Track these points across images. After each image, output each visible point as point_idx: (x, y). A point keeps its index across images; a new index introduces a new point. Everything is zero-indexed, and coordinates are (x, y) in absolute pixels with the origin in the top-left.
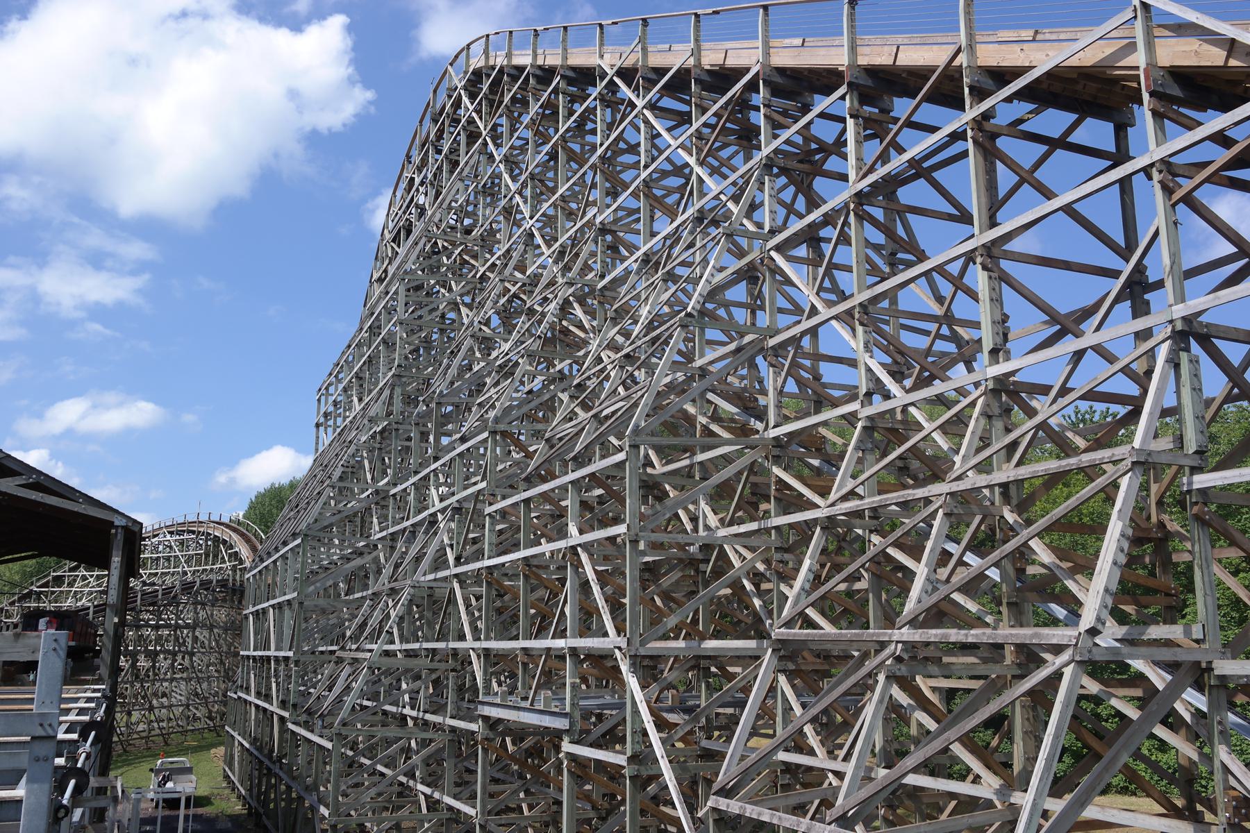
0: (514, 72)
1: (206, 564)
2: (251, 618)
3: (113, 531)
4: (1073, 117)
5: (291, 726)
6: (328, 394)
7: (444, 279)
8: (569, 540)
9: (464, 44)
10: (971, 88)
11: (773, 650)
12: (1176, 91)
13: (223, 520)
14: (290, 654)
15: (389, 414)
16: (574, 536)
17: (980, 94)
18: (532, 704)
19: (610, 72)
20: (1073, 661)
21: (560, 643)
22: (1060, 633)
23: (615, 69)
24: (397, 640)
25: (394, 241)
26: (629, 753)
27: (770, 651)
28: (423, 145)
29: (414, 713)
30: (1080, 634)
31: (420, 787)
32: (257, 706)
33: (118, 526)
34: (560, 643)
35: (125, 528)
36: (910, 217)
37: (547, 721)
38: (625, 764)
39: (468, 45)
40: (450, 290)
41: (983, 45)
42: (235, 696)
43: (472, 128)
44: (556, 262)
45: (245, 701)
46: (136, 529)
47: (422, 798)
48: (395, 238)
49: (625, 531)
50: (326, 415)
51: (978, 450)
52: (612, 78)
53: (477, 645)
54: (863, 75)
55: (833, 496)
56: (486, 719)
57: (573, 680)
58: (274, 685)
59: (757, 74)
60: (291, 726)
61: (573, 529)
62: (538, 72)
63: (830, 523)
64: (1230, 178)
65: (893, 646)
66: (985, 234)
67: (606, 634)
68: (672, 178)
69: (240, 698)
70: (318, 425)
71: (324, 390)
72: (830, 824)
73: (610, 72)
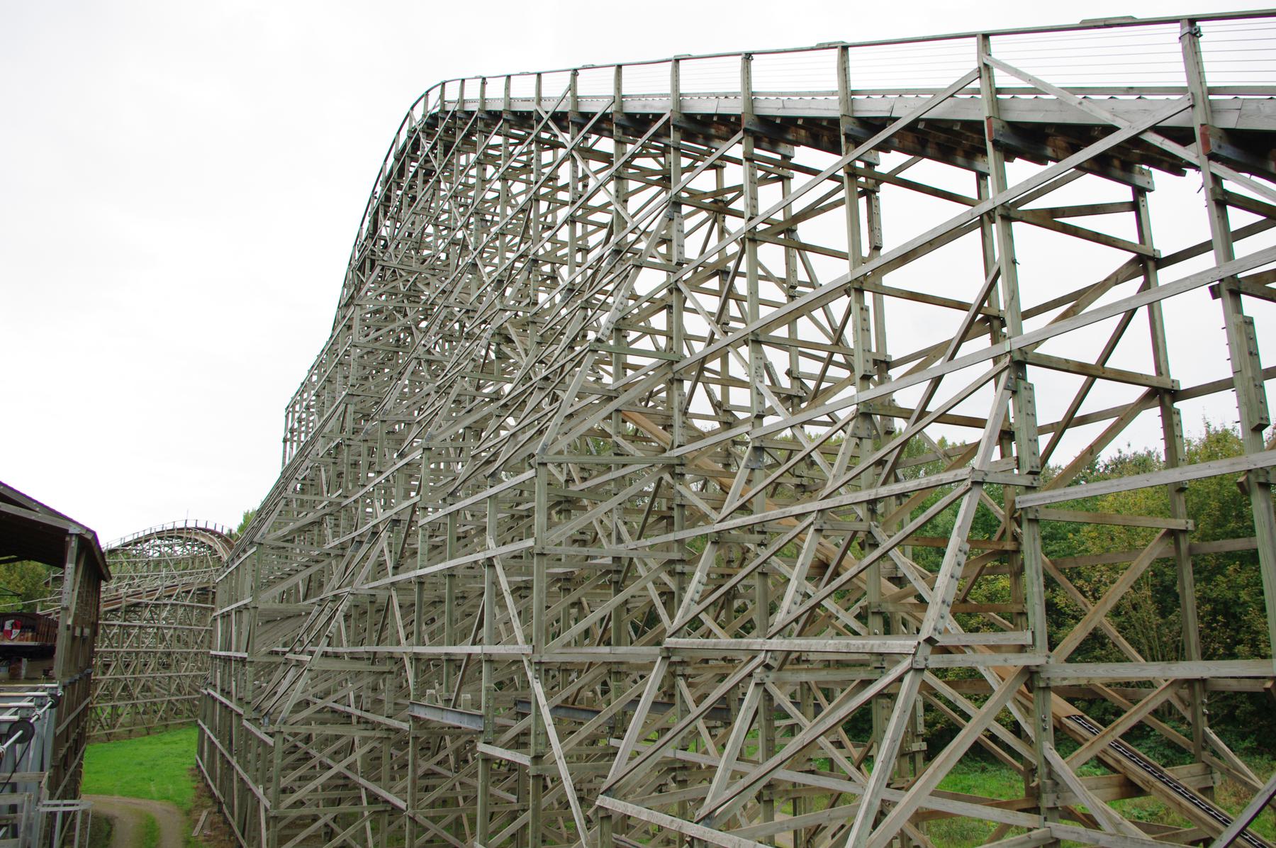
0: (463, 116)
1: (194, 568)
2: (219, 620)
3: (68, 539)
4: (594, 148)
5: (245, 723)
6: (294, 412)
7: (400, 305)
8: (488, 552)
9: (423, 92)
10: (847, 136)
11: (663, 658)
12: (1013, 142)
13: (209, 527)
14: (245, 655)
15: (342, 429)
16: (885, 544)
17: (856, 141)
18: (454, 707)
19: (546, 117)
20: (911, 669)
21: (477, 649)
22: (902, 642)
23: (549, 114)
24: (345, 643)
25: (359, 270)
26: (533, 755)
27: (660, 658)
28: (387, 182)
29: (358, 713)
30: (919, 643)
31: (362, 781)
32: (221, 703)
33: (72, 535)
34: (477, 649)
35: (80, 536)
36: (810, 256)
37: (466, 724)
38: (528, 763)
39: (428, 92)
40: (405, 315)
41: (624, 85)
42: (205, 692)
43: (428, 166)
44: (495, 290)
45: (213, 697)
46: (89, 537)
47: (363, 791)
48: (360, 267)
49: (533, 544)
50: (292, 431)
51: (849, 468)
52: (546, 123)
53: (409, 650)
54: (624, 118)
55: (725, 511)
56: (415, 719)
57: (488, 685)
58: (234, 683)
59: (668, 120)
60: (245, 723)
61: (490, 542)
62: (485, 116)
63: (719, 540)
64: (1064, 225)
65: (762, 655)
66: (857, 269)
67: (516, 643)
68: (599, 214)
69: (209, 694)
70: (285, 441)
71: (290, 409)
72: (697, 823)
73: (546, 117)
